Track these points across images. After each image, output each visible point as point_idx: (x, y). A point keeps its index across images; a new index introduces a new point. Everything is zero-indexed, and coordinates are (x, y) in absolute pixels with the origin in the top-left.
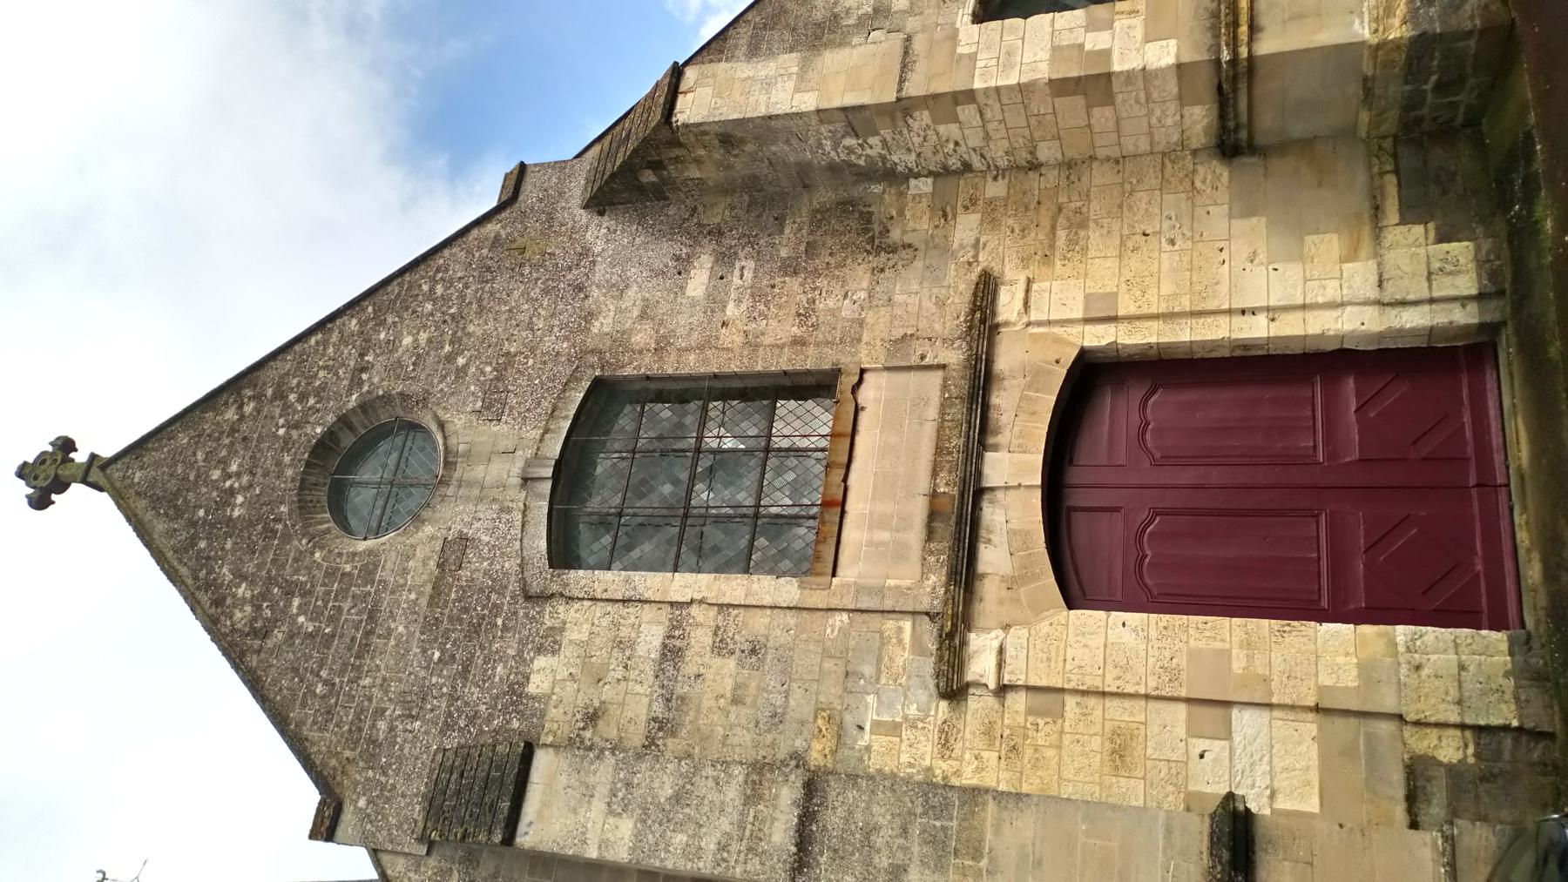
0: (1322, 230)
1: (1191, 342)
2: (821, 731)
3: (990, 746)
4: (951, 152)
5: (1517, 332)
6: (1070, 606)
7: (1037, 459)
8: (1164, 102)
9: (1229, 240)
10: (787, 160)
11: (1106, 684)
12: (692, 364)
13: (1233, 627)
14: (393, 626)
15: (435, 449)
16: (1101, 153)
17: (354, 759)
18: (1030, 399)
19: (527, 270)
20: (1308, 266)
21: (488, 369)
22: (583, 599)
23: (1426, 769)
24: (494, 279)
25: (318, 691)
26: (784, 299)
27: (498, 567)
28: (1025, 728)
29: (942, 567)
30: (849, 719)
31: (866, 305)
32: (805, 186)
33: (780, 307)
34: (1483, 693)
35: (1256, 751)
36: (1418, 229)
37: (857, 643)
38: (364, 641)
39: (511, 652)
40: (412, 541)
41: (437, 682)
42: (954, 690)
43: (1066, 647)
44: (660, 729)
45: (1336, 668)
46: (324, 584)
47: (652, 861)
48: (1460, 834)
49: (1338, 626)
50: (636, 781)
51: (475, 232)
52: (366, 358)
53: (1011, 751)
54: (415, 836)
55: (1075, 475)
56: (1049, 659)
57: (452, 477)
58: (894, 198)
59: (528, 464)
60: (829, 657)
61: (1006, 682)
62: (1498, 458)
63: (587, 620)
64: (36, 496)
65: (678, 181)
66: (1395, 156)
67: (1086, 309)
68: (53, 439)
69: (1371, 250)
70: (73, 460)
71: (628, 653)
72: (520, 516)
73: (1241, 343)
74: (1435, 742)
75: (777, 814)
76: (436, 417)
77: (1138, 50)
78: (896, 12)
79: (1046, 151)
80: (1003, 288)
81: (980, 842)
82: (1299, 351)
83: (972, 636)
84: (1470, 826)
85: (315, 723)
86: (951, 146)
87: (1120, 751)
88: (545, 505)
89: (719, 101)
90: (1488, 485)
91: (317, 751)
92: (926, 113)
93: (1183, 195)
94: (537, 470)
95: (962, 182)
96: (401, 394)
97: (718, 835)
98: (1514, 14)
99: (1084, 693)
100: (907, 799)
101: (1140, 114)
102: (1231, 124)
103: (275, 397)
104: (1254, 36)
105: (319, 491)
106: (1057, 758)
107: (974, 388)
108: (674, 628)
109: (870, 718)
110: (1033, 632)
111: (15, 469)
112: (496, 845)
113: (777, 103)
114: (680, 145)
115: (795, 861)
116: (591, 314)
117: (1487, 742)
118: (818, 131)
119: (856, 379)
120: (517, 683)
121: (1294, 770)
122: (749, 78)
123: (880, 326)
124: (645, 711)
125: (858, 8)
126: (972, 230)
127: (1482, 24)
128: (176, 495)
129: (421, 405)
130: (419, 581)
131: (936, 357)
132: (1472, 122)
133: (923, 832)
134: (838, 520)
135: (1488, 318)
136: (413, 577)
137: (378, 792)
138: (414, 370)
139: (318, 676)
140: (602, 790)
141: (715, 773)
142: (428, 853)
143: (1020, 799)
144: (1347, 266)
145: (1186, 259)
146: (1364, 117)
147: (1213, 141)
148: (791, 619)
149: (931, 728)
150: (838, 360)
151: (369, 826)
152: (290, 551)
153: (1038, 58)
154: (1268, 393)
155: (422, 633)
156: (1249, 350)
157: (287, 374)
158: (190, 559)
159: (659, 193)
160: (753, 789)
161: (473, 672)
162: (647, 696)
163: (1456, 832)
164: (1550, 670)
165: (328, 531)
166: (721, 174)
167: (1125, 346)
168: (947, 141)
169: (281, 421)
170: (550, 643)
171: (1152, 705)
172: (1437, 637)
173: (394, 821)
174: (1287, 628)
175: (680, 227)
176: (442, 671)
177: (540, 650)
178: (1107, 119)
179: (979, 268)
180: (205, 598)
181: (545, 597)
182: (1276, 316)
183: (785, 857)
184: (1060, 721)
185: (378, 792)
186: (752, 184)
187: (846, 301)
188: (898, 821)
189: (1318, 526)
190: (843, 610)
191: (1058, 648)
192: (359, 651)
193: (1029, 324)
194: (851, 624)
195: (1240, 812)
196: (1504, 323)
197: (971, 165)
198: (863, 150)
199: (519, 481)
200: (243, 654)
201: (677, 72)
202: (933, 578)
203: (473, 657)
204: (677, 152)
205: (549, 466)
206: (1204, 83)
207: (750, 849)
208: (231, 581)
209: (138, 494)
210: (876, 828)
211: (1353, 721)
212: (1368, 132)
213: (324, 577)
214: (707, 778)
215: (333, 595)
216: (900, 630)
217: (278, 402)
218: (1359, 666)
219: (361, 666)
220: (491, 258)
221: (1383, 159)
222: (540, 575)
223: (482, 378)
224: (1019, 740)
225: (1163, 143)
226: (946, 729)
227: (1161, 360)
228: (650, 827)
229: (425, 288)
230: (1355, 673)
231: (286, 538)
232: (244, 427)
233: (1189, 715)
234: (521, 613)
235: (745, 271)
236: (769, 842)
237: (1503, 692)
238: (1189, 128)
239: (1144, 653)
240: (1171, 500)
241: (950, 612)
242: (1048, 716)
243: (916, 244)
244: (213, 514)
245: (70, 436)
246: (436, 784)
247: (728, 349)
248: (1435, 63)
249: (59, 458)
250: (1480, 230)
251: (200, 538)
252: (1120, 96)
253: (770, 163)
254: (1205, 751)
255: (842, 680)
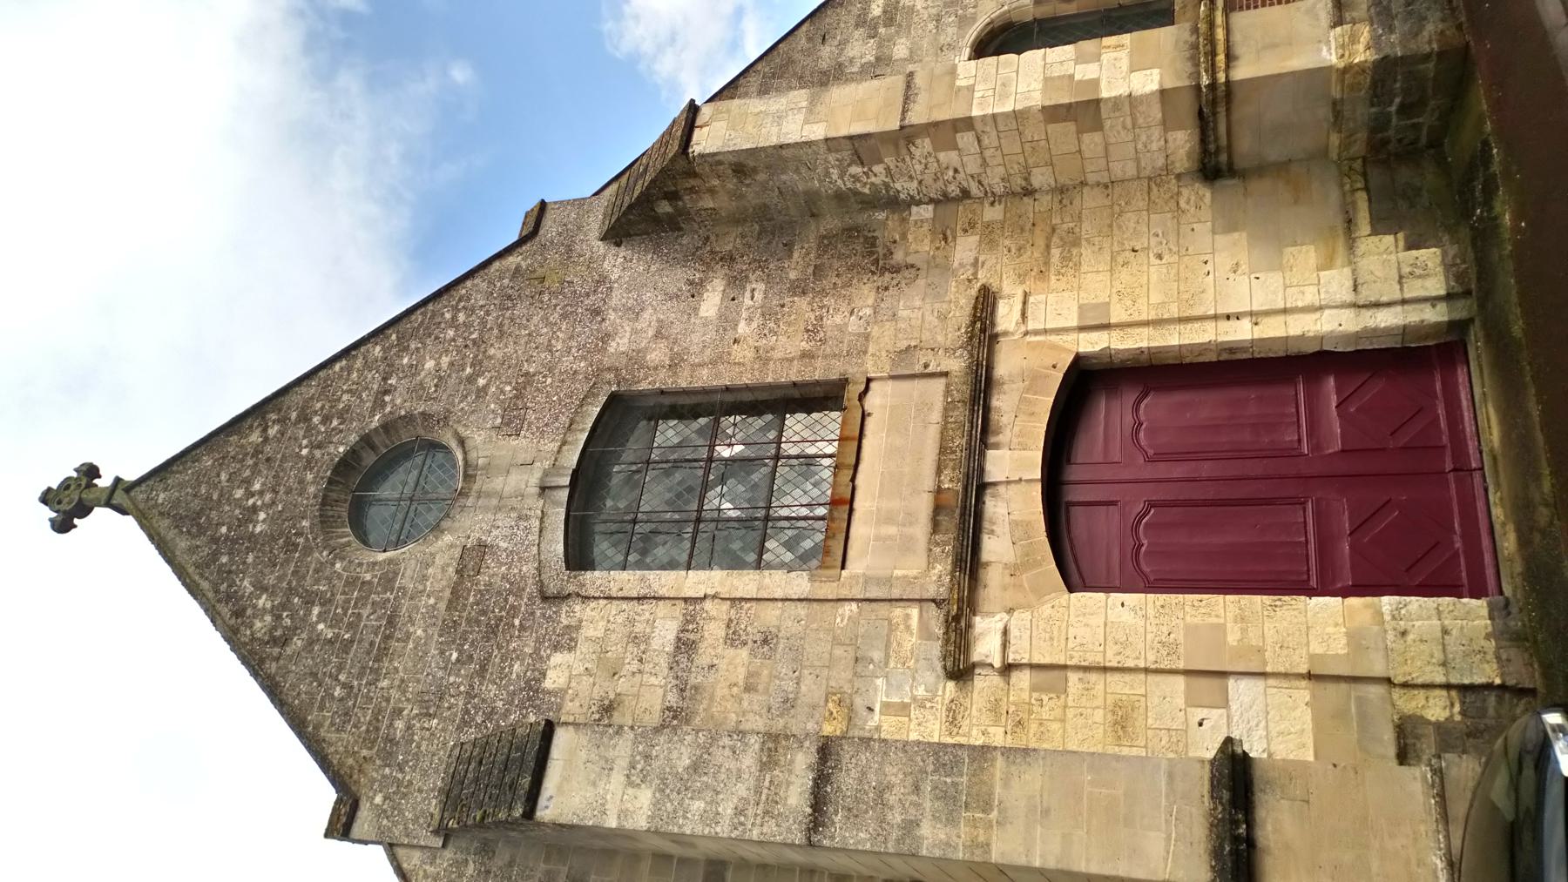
0: (1299, 242)
1: (1180, 346)
2: (832, 713)
3: (996, 723)
4: (951, 179)
5: (1484, 325)
6: (1071, 589)
7: (1037, 456)
8: (1149, 127)
9: (1213, 253)
10: (796, 189)
11: (1107, 659)
12: (705, 378)
13: (1227, 603)
14: (412, 630)
15: (454, 466)
16: (1091, 178)
17: (371, 758)
18: (1029, 402)
19: (546, 298)
20: (1288, 274)
21: (508, 388)
22: (599, 598)
23: (1415, 727)
24: (514, 306)
25: (336, 694)
26: (793, 317)
27: (516, 571)
28: (1030, 704)
29: (947, 556)
30: (859, 702)
31: (873, 320)
32: (813, 215)
33: (789, 324)
34: (1466, 655)
35: (1253, 717)
36: (1389, 239)
37: (867, 631)
38: (383, 646)
39: (528, 650)
40: (432, 549)
41: (455, 682)
42: (960, 671)
43: (1068, 626)
44: (674, 717)
45: (1326, 637)
46: (344, 593)
47: (671, 827)
48: (1447, 767)
49: (1327, 599)
50: (654, 753)
51: (497, 265)
52: (389, 382)
53: (1017, 726)
54: (431, 829)
55: (1073, 473)
56: (1051, 639)
57: (470, 489)
58: (897, 223)
59: (546, 474)
60: (839, 644)
61: (1010, 661)
62: (1472, 446)
63: (603, 617)
64: (59, 519)
65: (691, 210)
66: (1364, 175)
67: (1081, 316)
68: (77, 465)
69: (1346, 260)
70: (96, 486)
71: (642, 648)
72: (538, 523)
73: (1227, 347)
74: (1423, 702)
75: (793, 779)
76: (456, 434)
77: (1124, 78)
78: (896, 60)
79: (1041, 177)
80: (1001, 301)
81: (990, 795)
82: (1281, 354)
83: (977, 620)
84: (1457, 759)
85: (332, 724)
86: (951, 173)
87: (1122, 721)
88: (562, 511)
89: (733, 133)
90: (1462, 469)
91: (335, 752)
92: (927, 141)
93: (1169, 215)
94: (555, 479)
95: (961, 208)
96: (423, 414)
97: (735, 801)
98: (1468, 38)
99: (1086, 669)
100: (919, 759)
101: (1127, 139)
102: (1212, 147)
103: (298, 421)
104: (1231, 65)
105: (341, 507)
106: (1061, 731)
107: (975, 390)
108: (688, 622)
109: (879, 699)
110: (1036, 614)
111: (39, 495)
112: (517, 819)
113: (788, 133)
114: (695, 175)
115: (811, 822)
116: (608, 335)
117: (1473, 700)
118: (826, 160)
119: (863, 387)
120: (534, 679)
121: (1289, 734)
122: (761, 112)
123: (885, 339)
124: (660, 701)
125: (861, 57)
126: (971, 251)
127: (1439, 48)
128: (199, 514)
129: (442, 423)
130: (438, 587)
131: (938, 365)
132: (1435, 143)
133: (935, 788)
134: (846, 517)
135: (1457, 316)
136: (432, 583)
137: (394, 789)
138: (436, 391)
139: (337, 679)
140: (622, 763)
141: (731, 743)
142: (444, 846)
143: (1027, 754)
144: (1322, 274)
145: (1174, 271)
146: (1335, 139)
147: (1196, 166)
148: (802, 609)
149: (939, 707)
150: (845, 371)
151: (385, 822)
152: (311, 562)
153: (1031, 88)
154: (1252, 393)
155: (441, 636)
156: (1234, 353)
157: (312, 398)
158: (212, 574)
159: (673, 224)
160: (769, 756)
161: (490, 670)
162: (661, 687)
163: (1443, 764)
164: (1528, 630)
165: (348, 544)
166: (734, 204)
167: (1118, 351)
168: (947, 168)
169: (305, 442)
170: (566, 640)
171: (1152, 678)
172: (1420, 606)
173: (410, 816)
174: (1278, 603)
175: (693, 254)
176: (459, 670)
177: (556, 647)
178: (1096, 145)
179: (979, 284)
180: (225, 610)
181: (561, 598)
182: (1259, 320)
183: (800, 818)
184: (1063, 696)
185: (394, 789)
186: (762, 214)
187: (853, 317)
188: (910, 780)
189: (1304, 512)
190: (852, 600)
191: (1060, 627)
192: (378, 655)
193: (1026, 334)
194: (860, 614)
195: (1238, 755)
196: (1471, 320)
197: (969, 192)
198: (868, 178)
199: (537, 490)
200: (262, 661)
201: (693, 109)
202: (939, 567)
203: (490, 656)
204: (693, 182)
205: (566, 475)
206: (1186, 108)
207: (766, 813)
208: (251, 593)
209: (161, 514)
210: (889, 787)
211: (1344, 686)
212: (1339, 154)
213: (344, 586)
214: (724, 747)
215: (353, 602)
216: (908, 617)
217: (302, 425)
218: (1347, 634)
219: (379, 668)
220: (512, 287)
221: (1354, 178)
222: (557, 576)
223: (502, 397)
224: (1025, 716)
225: (1149, 168)
226: (954, 707)
227: (1152, 366)
228: (668, 795)
229: (448, 316)
230: (1344, 641)
231: (308, 551)
232: (268, 449)
233: (1188, 686)
234: (538, 613)
235: (756, 293)
236: (785, 805)
237: (1485, 653)
238: (1173, 153)
239: (1142, 630)
240: (1161, 494)
241: (956, 596)
242: (1053, 692)
243: (918, 264)
244: (235, 531)
245: (95, 463)
246: (453, 777)
247: (739, 364)
248: (1398, 85)
249: (84, 483)
250: (1446, 238)
251: (222, 554)
252: (1109, 122)
253: (781, 192)
254: (1203, 719)
255: (851, 667)
